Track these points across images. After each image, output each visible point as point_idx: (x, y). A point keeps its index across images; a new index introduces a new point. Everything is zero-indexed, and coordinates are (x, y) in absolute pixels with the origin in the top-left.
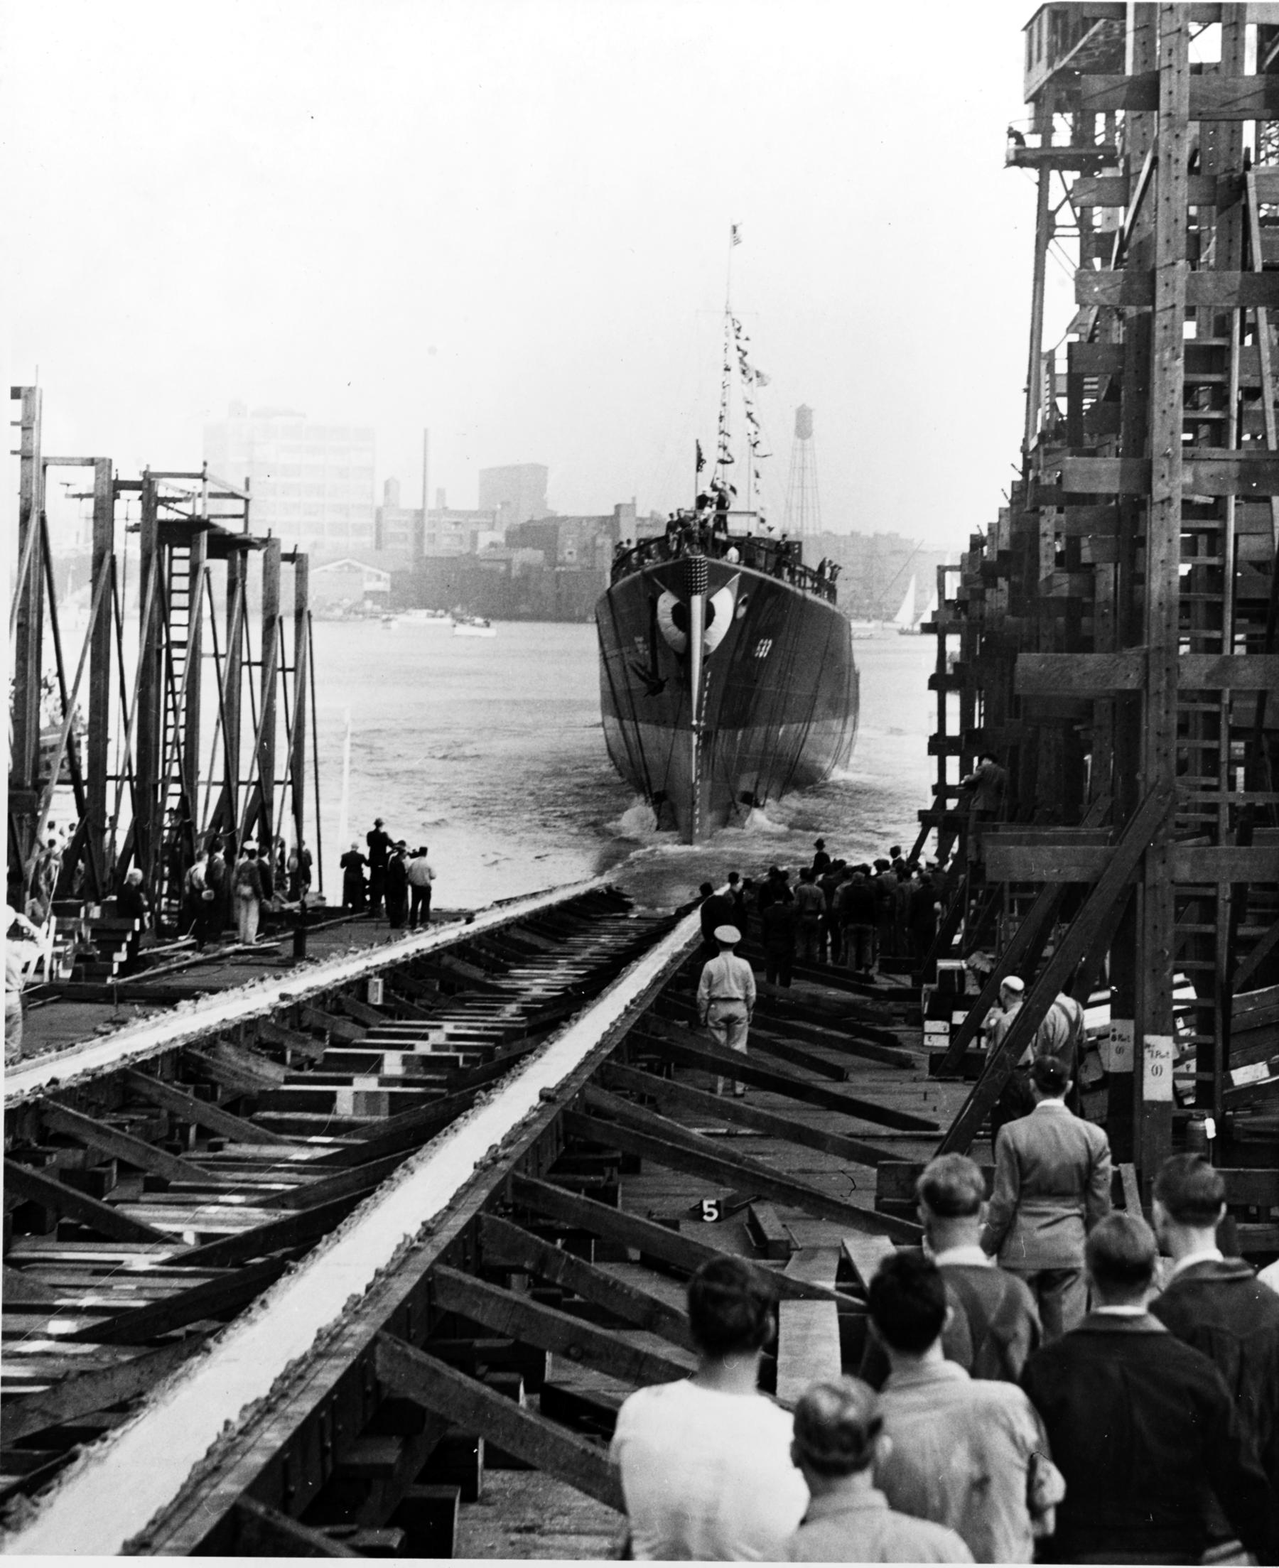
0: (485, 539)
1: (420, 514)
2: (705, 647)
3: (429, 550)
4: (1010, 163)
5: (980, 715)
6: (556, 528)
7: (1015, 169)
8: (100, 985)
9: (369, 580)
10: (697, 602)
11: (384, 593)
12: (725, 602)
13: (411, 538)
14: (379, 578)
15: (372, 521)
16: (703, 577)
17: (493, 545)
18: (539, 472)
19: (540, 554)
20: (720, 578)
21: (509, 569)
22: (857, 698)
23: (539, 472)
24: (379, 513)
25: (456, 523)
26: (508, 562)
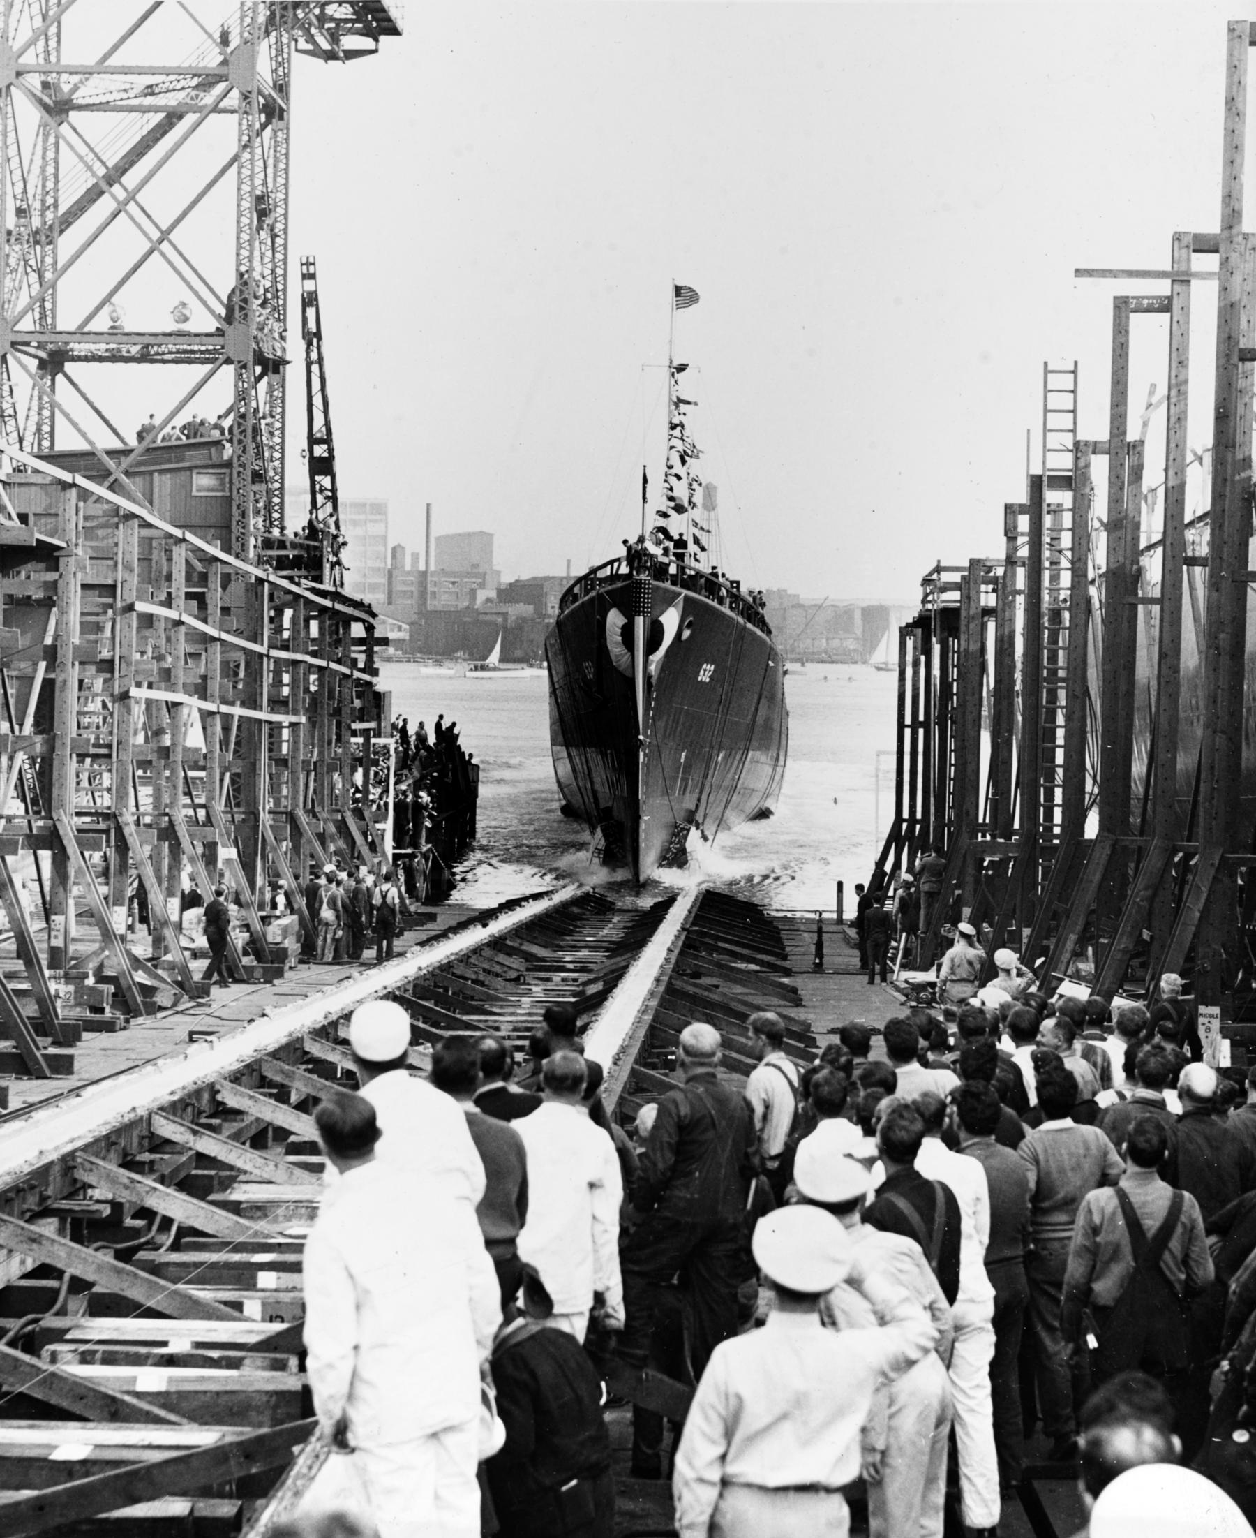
0: (481, 596)
1: (424, 574)
2: (647, 678)
3: (431, 604)
4: (395, 31)
5: (269, 671)
6: (542, 587)
7: (400, 25)
8: (1101, 856)
9: (392, 630)
10: (640, 622)
11: (404, 640)
12: (671, 620)
13: (416, 594)
14: (400, 629)
15: (384, 581)
16: (648, 599)
17: (488, 600)
18: (485, 539)
19: (531, 608)
20: (669, 600)
21: (505, 620)
22: (1218, 359)
23: (485, 539)
24: (390, 573)
25: (453, 583)
26: (505, 615)
